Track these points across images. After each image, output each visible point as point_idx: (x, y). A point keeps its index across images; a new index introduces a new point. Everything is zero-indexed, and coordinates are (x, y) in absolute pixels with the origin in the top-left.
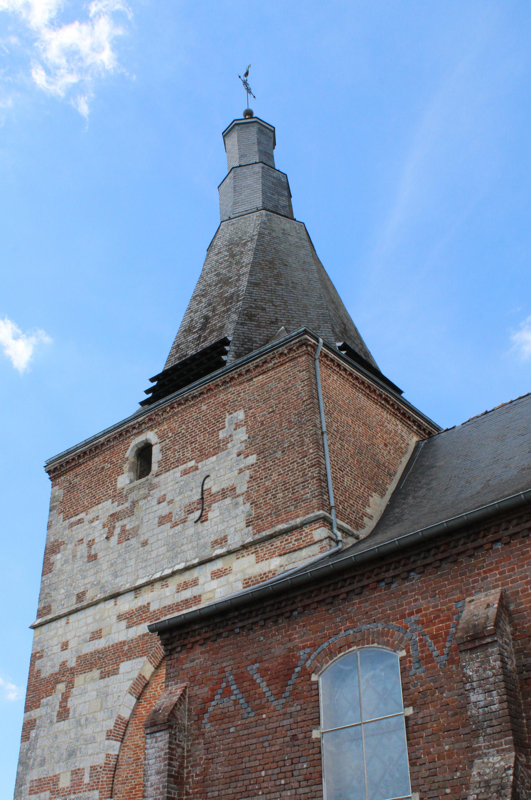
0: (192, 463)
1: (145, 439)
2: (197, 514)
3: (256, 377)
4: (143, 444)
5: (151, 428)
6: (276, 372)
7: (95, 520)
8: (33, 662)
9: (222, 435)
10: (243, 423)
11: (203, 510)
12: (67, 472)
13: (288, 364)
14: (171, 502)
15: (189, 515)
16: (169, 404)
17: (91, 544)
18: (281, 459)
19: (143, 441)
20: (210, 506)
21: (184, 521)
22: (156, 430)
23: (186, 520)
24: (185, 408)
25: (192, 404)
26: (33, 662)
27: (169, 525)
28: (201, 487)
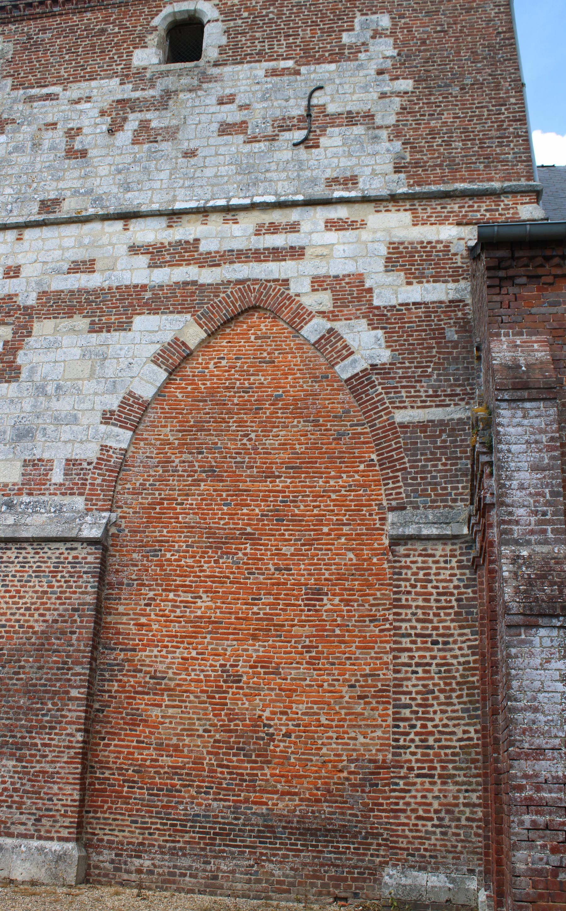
0: (290, 64)
1: (193, 8)
4: (186, 16)
7: (83, 102)
10: (388, 32)
12: (23, 20)
19: (188, 11)
21: (273, 139)
27: (241, 138)
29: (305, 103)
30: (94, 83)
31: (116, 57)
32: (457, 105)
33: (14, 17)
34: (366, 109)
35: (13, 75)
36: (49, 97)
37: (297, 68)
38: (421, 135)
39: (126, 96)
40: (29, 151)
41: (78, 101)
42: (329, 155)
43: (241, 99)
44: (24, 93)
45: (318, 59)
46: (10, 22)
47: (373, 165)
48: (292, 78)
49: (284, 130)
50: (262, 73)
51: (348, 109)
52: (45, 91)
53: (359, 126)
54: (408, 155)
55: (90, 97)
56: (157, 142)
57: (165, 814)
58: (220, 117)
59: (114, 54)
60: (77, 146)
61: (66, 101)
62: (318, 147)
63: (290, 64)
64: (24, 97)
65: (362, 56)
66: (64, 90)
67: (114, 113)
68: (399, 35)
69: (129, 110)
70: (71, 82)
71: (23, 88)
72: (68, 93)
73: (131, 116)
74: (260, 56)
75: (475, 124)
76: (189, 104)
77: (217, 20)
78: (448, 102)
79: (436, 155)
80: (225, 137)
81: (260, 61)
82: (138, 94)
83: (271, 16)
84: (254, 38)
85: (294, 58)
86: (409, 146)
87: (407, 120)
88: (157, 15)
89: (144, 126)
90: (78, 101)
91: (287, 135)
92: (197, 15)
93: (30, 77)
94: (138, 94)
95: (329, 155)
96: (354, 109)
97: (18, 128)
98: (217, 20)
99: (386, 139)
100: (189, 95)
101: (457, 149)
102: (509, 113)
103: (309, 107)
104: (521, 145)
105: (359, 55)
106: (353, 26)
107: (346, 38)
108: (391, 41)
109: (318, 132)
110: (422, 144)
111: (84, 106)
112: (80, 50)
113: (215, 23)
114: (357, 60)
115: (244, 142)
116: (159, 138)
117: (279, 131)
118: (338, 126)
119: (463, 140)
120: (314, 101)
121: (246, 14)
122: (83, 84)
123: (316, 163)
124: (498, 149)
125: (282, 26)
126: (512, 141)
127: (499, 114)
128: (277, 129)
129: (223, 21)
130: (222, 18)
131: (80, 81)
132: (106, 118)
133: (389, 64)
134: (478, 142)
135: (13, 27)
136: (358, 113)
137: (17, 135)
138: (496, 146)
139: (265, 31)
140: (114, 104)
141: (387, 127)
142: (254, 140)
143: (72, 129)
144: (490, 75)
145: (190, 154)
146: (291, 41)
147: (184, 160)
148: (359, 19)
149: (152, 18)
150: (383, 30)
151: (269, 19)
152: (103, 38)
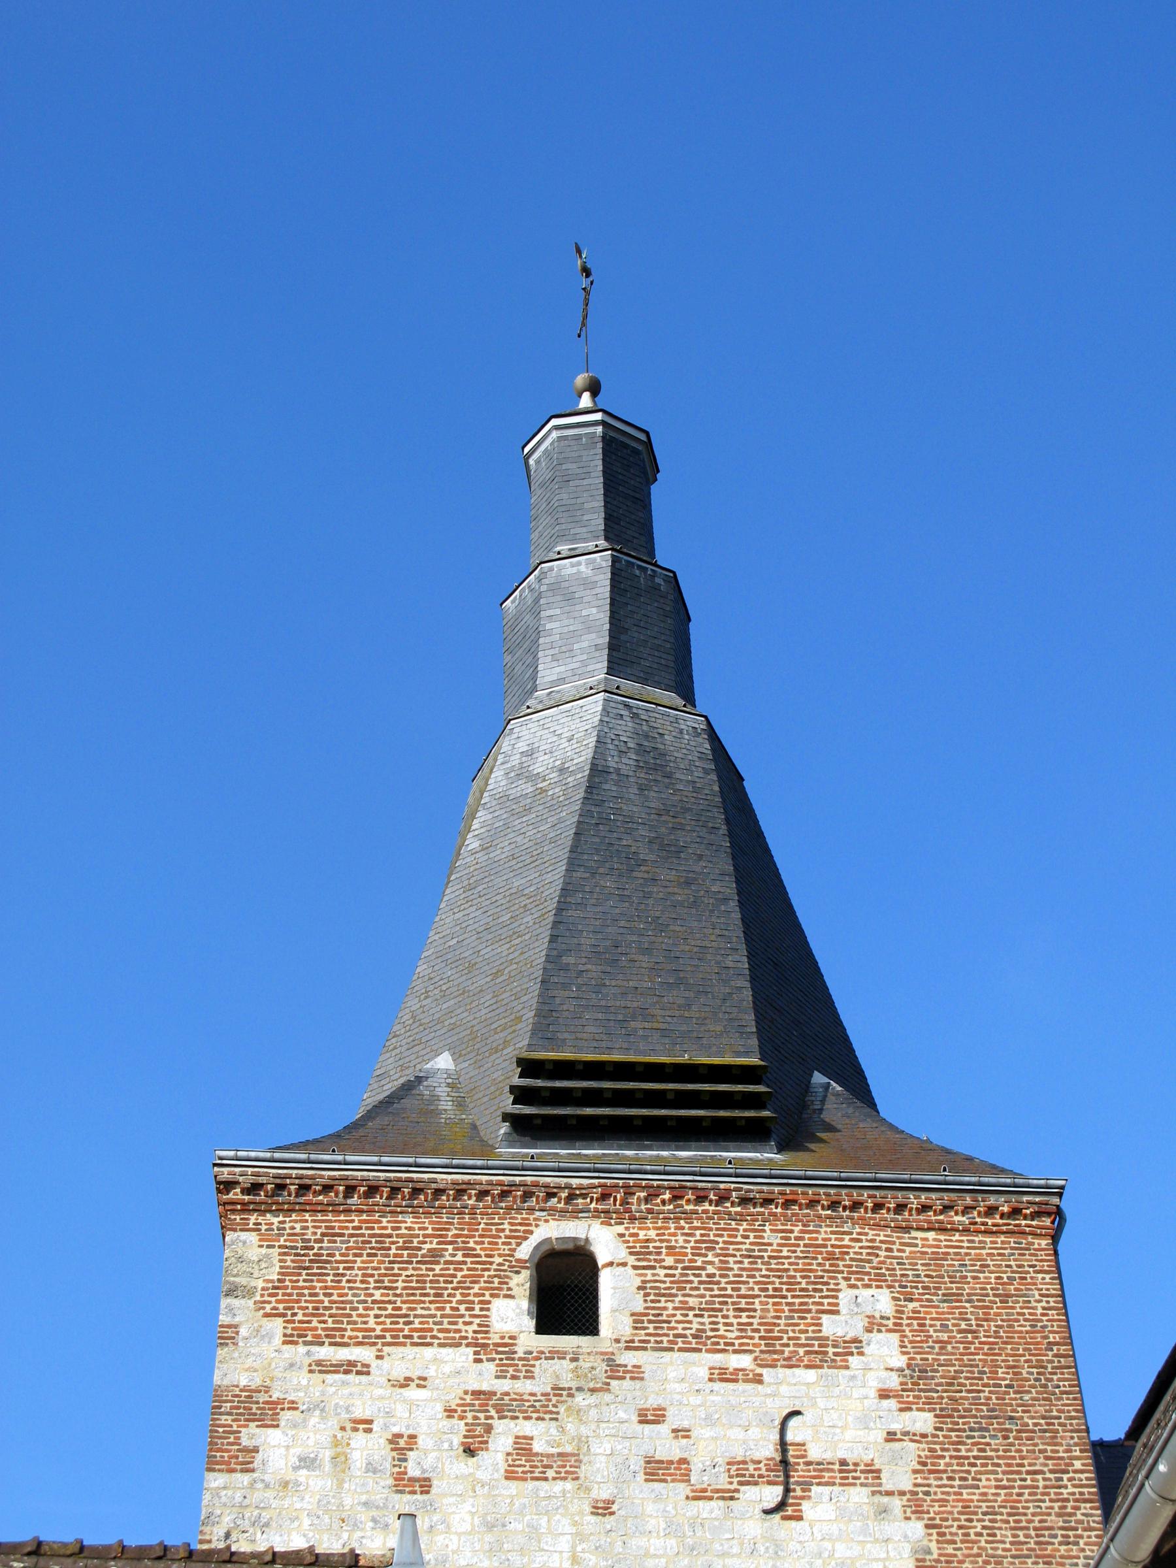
0: (744, 1361)
1: (583, 1236)
2: (772, 1494)
3: (919, 1229)
4: (570, 1246)
5: (606, 1217)
6: (973, 1241)
7: (413, 1385)
9: (831, 1327)
10: (890, 1323)
11: (787, 1490)
12: (293, 1210)
13: (1003, 1238)
14: (681, 1433)
15: (742, 1488)
16: (677, 1184)
17: (402, 1445)
18: (930, 1439)
19: (575, 1239)
20: (806, 1486)
21: (729, 1496)
22: (620, 1229)
23: (736, 1495)
24: (715, 1213)
25: (736, 1213)
27: (683, 1489)
28: (777, 1430)
29: (775, 1436)
30: (428, 1352)
31: (462, 1307)
32: (998, 1465)
33: (277, 1203)
34: (867, 1458)
35: (284, 1315)
36: (348, 1367)
37: (759, 1370)
38: (951, 1513)
39: (485, 1387)
40: (327, 1467)
41: (406, 1383)
42: (818, 1536)
43: (675, 1419)
44: (308, 1353)
45: (789, 1359)
46: (270, 1211)
47: (884, 1559)
48: (750, 1387)
49: (748, 1483)
50: (704, 1373)
51: (841, 1454)
52: (344, 1354)
53: (858, 1489)
54: (933, 1546)
55: (425, 1379)
56: (546, 1479)
58: (646, 1448)
59: (460, 1302)
60: (413, 1471)
61: (384, 1380)
62: (800, 1518)
63: (744, 1361)
64: (307, 1361)
65: (854, 1361)
66: (379, 1357)
67: (469, 1415)
68: (907, 1329)
69: (493, 1413)
71: (306, 1343)
72: (385, 1364)
73: (499, 1425)
74: (699, 1342)
77: (624, 1264)
78: (986, 1458)
79: (975, 1551)
81: (700, 1350)
82: (505, 1385)
83: (710, 1269)
84: (685, 1307)
85: (751, 1352)
86: (934, 1531)
88: (526, 1239)
89: (523, 1447)
90: (406, 1383)
91: (749, 1493)
92: (587, 1247)
93: (315, 1324)
94: (505, 1385)
95: (818, 1536)
96: (851, 1457)
97: (305, 1420)
98: (624, 1264)
99: (901, 1515)
100: (592, 1399)
102: (1074, 1486)
103: (783, 1445)
104: (1094, 1544)
105: (850, 1358)
106: (837, 1305)
107: (831, 1327)
108: (895, 1338)
109: (799, 1493)
111: (413, 1393)
112: (400, 1284)
113: (621, 1269)
116: (550, 1473)
117: (741, 1483)
118: (827, 1484)
119: (1012, 1529)
120: (779, 1490)
121: (670, 1261)
122: (409, 1351)
123: (799, 1547)
124: (1063, 1548)
125: (729, 1292)
126: (1081, 1537)
127: (1060, 1487)
128: (735, 1480)
129: (635, 1267)
130: (632, 1260)
131: (404, 1344)
132: (455, 1421)
133: (894, 1382)
134: (1033, 1533)
135: (275, 1220)
138: (1060, 1544)
139: (703, 1296)
140: (468, 1398)
141: (902, 1493)
142: (700, 1495)
143: (400, 1436)
144: (1044, 1417)
145: (603, 1509)
146: (744, 1320)
147: (593, 1519)
148: (845, 1297)
149: (519, 1244)
150: (882, 1318)
151: (708, 1276)
152: (437, 1268)
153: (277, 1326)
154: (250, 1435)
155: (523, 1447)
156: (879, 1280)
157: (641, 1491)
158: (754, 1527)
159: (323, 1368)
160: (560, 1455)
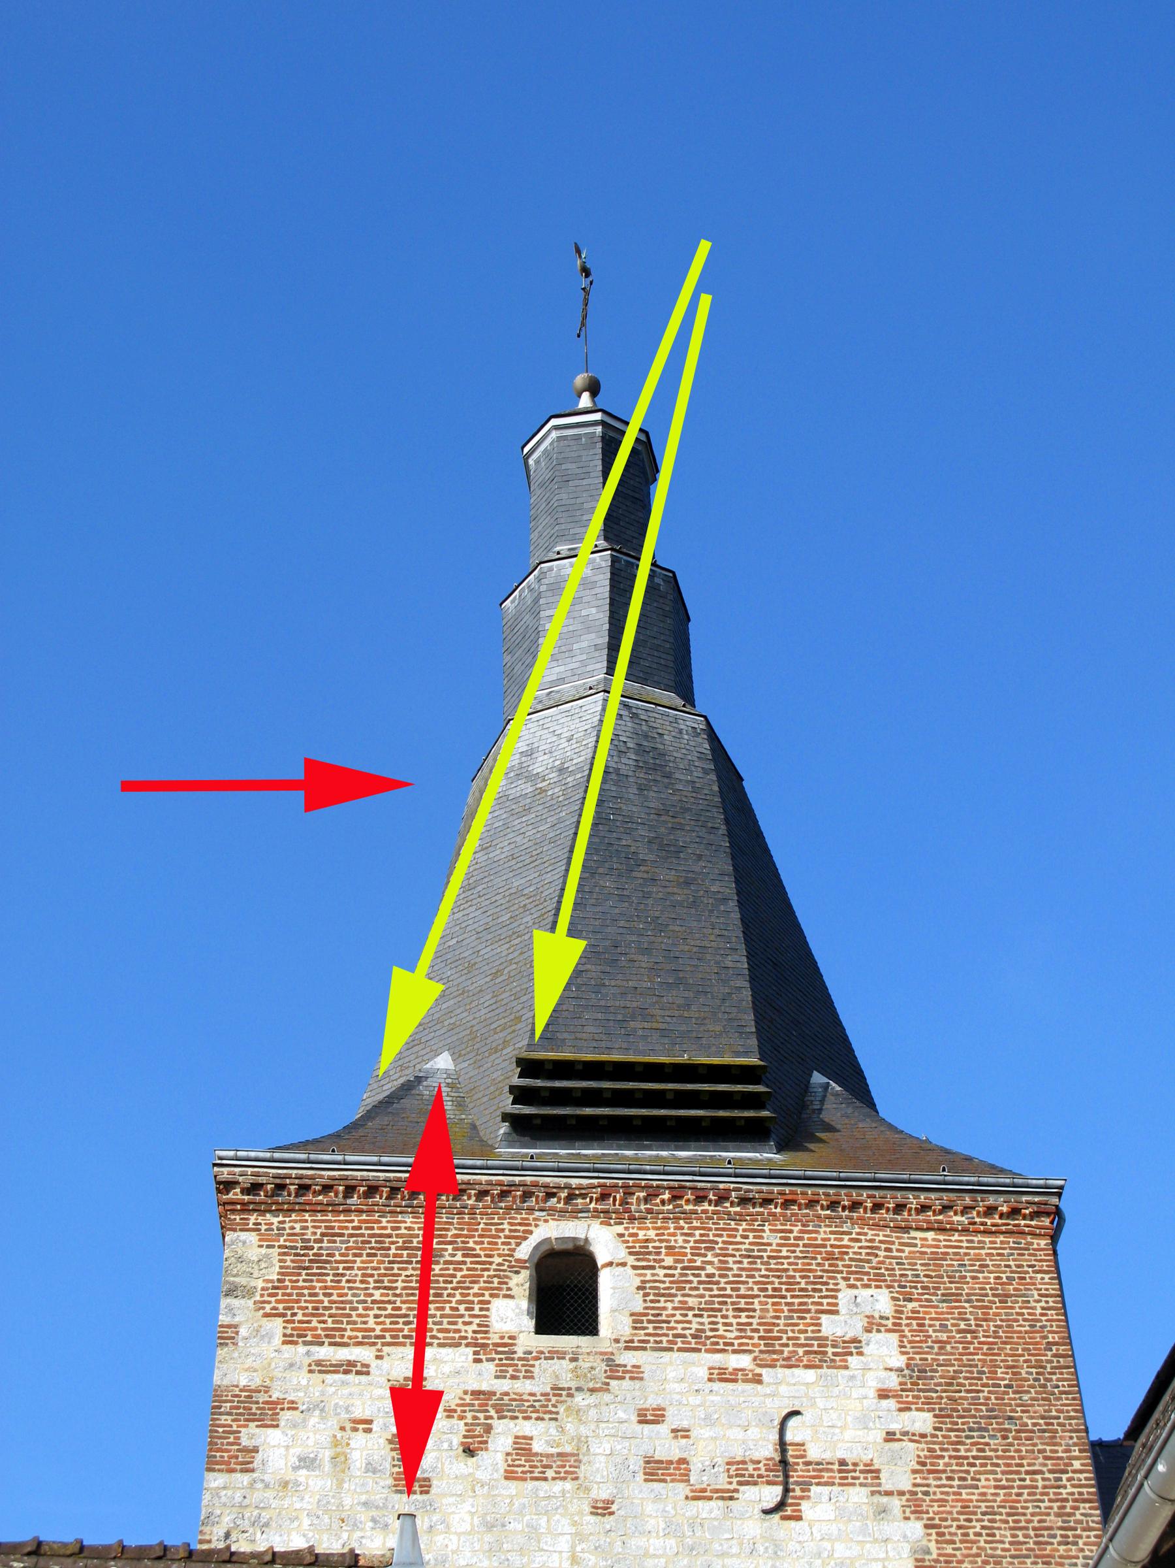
0: (744, 1361)
1: (583, 1236)
2: (771, 1494)
3: (918, 1229)
4: (570, 1246)
5: (605, 1217)
6: (972, 1241)
8: (373, 1115)
9: (830, 1327)
10: (889, 1323)
12: (293, 1210)
14: (680, 1433)
16: (676, 1184)
19: (574, 1239)
20: (805, 1486)
21: (728, 1496)
22: (620, 1229)
23: (736, 1495)
26: (373, 1115)
27: (682, 1489)
28: (777, 1430)
29: (774, 1436)
31: (462, 1307)
32: (998, 1465)
33: (277, 1203)
34: (866, 1458)
35: (284, 1315)
36: (348, 1367)
37: (758, 1370)
38: (950, 1513)
39: (485, 1387)
40: (327, 1467)
42: (817, 1536)
43: (674, 1419)
44: (308, 1353)
45: (788, 1359)
46: (270, 1211)
47: (884, 1559)
48: (749, 1387)
49: (747, 1483)
50: (703, 1373)
51: (840, 1454)
52: (344, 1354)
53: (858, 1489)
54: (933, 1546)
56: (545, 1479)
57: (1007, 1480)
58: (646, 1448)
59: (460, 1302)
62: (799, 1518)
63: (744, 1361)
65: (853, 1361)
66: (379, 1357)
67: (469, 1415)
68: (906, 1329)
69: (492, 1413)
70: (389, 1344)
71: (305, 1343)
72: (385, 1364)
73: (499, 1425)
74: (698, 1342)
75: (1026, 1501)
76: (593, 1413)
77: (624, 1264)
79: (974, 1551)
80: (655, 1485)
81: (699, 1350)
82: (504, 1385)
83: (710, 1269)
84: (685, 1307)
85: (750, 1352)
86: (933, 1531)
87: (928, 1485)
88: (526, 1239)
89: (522, 1447)
91: (748, 1493)
92: (587, 1247)
93: (314, 1324)
94: (504, 1385)
95: (817, 1536)
96: (850, 1457)
97: (304, 1420)
98: (624, 1264)
99: (900, 1515)
100: (591, 1399)
101: (1003, 1542)
102: (1073, 1486)
103: (782, 1445)
104: (1093, 1544)
105: (849, 1358)
106: (836, 1305)
108: (894, 1338)
109: (798, 1493)
110: (953, 1530)
112: (400, 1284)
113: (621, 1269)
114: (846, 1367)
115: (687, 1498)
116: (550, 1473)
117: (740, 1483)
118: (826, 1484)
119: (1011, 1529)
121: (669, 1261)
123: (798, 1547)
125: (728, 1292)
126: (1080, 1537)
127: (1059, 1487)
128: (735, 1480)
129: (634, 1267)
130: (631, 1260)
132: (455, 1421)
133: (893, 1382)
134: (1032, 1533)
135: (275, 1220)
136: (855, 1464)
137: (303, 1434)
138: (1060, 1544)
139: (702, 1296)
140: (468, 1398)
141: (901, 1493)
142: (699, 1495)
144: (1043, 1417)
145: (603, 1509)
147: (593, 1519)
148: (845, 1297)
149: (518, 1244)
150: (881, 1318)
151: (708, 1276)
153: (277, 1326)
154: (250, 1435)
155: (522, 1447)
156: (878, 1280)
157: (640, 1491)
158: (754, 1527)
159: (322, 1368)
160: (559, 1455)
